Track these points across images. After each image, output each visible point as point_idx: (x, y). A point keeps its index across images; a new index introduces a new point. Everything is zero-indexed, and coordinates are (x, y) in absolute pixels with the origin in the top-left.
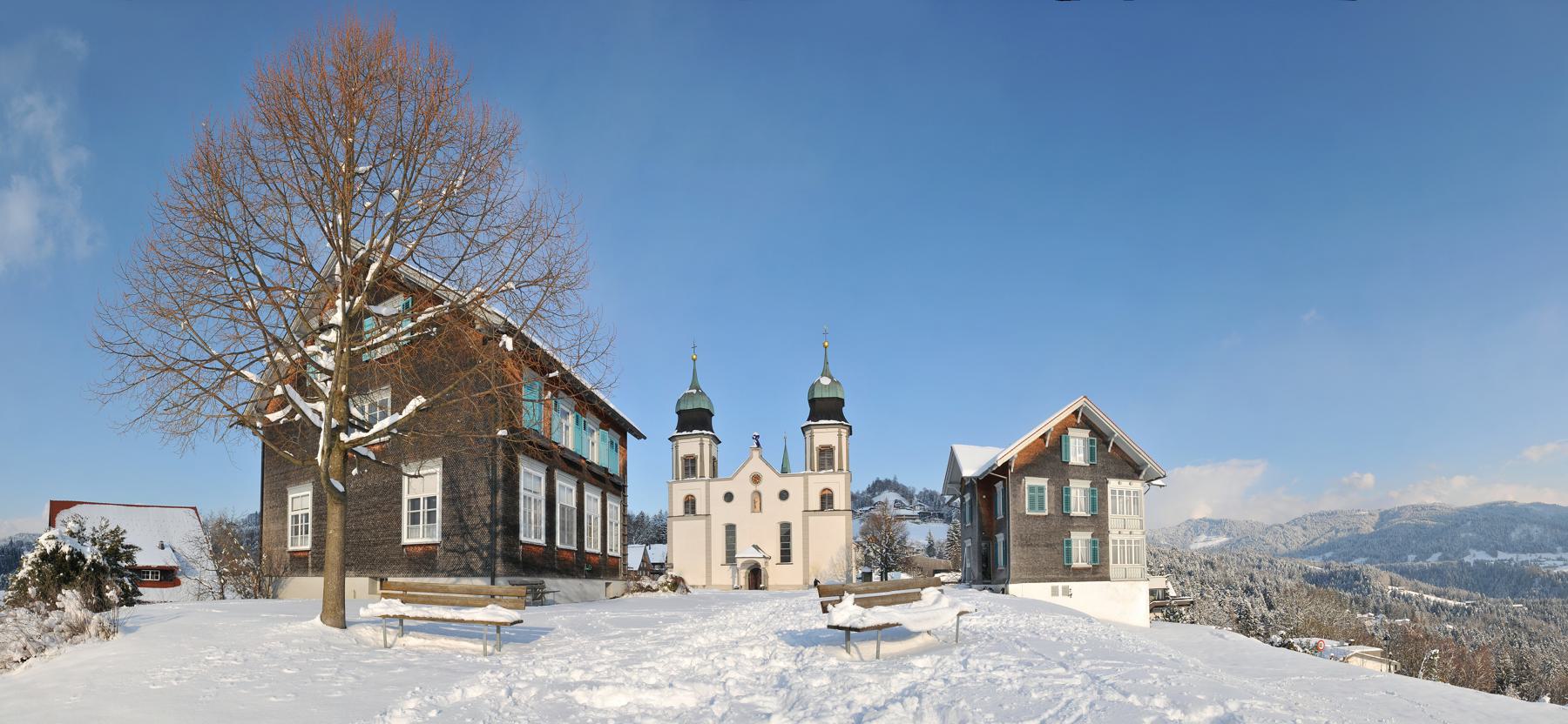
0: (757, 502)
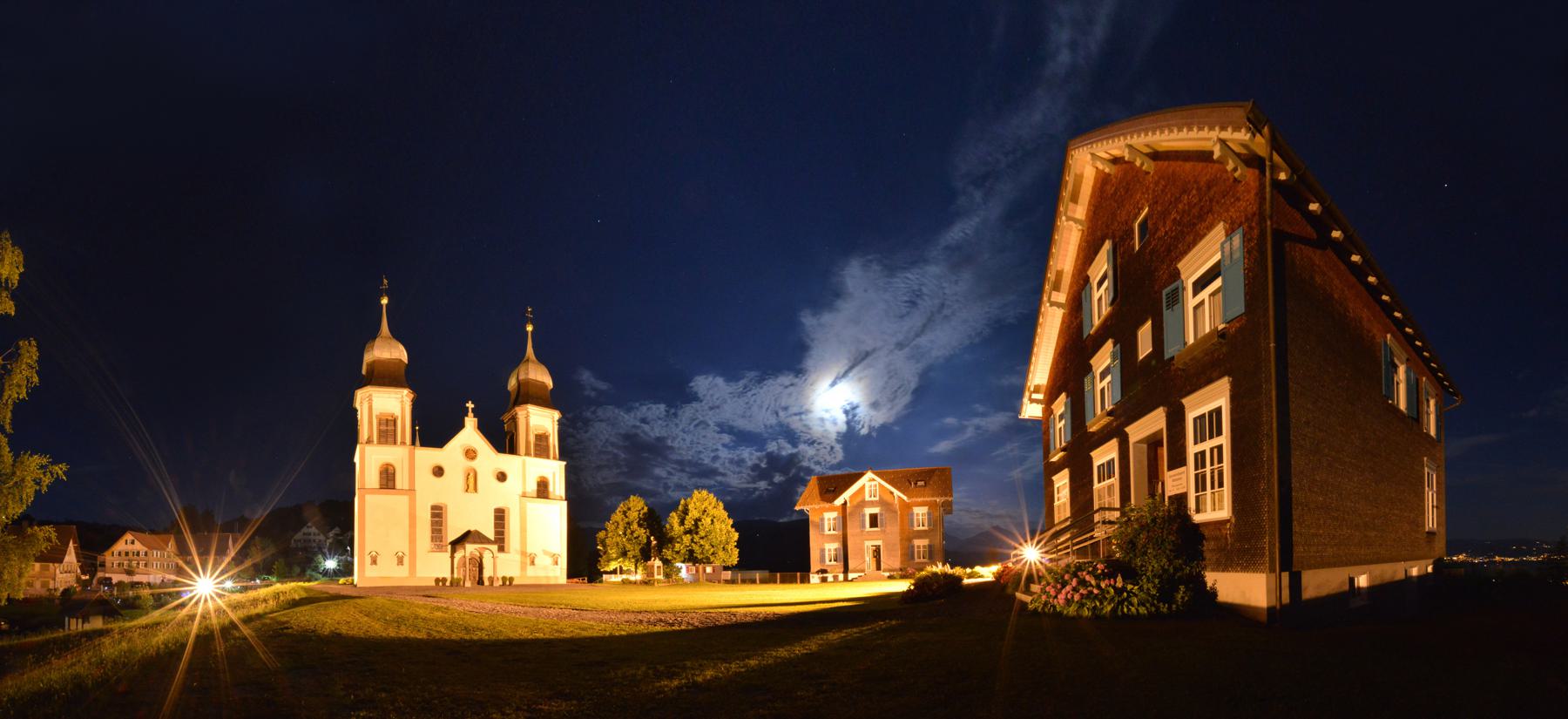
0: (471, 482)
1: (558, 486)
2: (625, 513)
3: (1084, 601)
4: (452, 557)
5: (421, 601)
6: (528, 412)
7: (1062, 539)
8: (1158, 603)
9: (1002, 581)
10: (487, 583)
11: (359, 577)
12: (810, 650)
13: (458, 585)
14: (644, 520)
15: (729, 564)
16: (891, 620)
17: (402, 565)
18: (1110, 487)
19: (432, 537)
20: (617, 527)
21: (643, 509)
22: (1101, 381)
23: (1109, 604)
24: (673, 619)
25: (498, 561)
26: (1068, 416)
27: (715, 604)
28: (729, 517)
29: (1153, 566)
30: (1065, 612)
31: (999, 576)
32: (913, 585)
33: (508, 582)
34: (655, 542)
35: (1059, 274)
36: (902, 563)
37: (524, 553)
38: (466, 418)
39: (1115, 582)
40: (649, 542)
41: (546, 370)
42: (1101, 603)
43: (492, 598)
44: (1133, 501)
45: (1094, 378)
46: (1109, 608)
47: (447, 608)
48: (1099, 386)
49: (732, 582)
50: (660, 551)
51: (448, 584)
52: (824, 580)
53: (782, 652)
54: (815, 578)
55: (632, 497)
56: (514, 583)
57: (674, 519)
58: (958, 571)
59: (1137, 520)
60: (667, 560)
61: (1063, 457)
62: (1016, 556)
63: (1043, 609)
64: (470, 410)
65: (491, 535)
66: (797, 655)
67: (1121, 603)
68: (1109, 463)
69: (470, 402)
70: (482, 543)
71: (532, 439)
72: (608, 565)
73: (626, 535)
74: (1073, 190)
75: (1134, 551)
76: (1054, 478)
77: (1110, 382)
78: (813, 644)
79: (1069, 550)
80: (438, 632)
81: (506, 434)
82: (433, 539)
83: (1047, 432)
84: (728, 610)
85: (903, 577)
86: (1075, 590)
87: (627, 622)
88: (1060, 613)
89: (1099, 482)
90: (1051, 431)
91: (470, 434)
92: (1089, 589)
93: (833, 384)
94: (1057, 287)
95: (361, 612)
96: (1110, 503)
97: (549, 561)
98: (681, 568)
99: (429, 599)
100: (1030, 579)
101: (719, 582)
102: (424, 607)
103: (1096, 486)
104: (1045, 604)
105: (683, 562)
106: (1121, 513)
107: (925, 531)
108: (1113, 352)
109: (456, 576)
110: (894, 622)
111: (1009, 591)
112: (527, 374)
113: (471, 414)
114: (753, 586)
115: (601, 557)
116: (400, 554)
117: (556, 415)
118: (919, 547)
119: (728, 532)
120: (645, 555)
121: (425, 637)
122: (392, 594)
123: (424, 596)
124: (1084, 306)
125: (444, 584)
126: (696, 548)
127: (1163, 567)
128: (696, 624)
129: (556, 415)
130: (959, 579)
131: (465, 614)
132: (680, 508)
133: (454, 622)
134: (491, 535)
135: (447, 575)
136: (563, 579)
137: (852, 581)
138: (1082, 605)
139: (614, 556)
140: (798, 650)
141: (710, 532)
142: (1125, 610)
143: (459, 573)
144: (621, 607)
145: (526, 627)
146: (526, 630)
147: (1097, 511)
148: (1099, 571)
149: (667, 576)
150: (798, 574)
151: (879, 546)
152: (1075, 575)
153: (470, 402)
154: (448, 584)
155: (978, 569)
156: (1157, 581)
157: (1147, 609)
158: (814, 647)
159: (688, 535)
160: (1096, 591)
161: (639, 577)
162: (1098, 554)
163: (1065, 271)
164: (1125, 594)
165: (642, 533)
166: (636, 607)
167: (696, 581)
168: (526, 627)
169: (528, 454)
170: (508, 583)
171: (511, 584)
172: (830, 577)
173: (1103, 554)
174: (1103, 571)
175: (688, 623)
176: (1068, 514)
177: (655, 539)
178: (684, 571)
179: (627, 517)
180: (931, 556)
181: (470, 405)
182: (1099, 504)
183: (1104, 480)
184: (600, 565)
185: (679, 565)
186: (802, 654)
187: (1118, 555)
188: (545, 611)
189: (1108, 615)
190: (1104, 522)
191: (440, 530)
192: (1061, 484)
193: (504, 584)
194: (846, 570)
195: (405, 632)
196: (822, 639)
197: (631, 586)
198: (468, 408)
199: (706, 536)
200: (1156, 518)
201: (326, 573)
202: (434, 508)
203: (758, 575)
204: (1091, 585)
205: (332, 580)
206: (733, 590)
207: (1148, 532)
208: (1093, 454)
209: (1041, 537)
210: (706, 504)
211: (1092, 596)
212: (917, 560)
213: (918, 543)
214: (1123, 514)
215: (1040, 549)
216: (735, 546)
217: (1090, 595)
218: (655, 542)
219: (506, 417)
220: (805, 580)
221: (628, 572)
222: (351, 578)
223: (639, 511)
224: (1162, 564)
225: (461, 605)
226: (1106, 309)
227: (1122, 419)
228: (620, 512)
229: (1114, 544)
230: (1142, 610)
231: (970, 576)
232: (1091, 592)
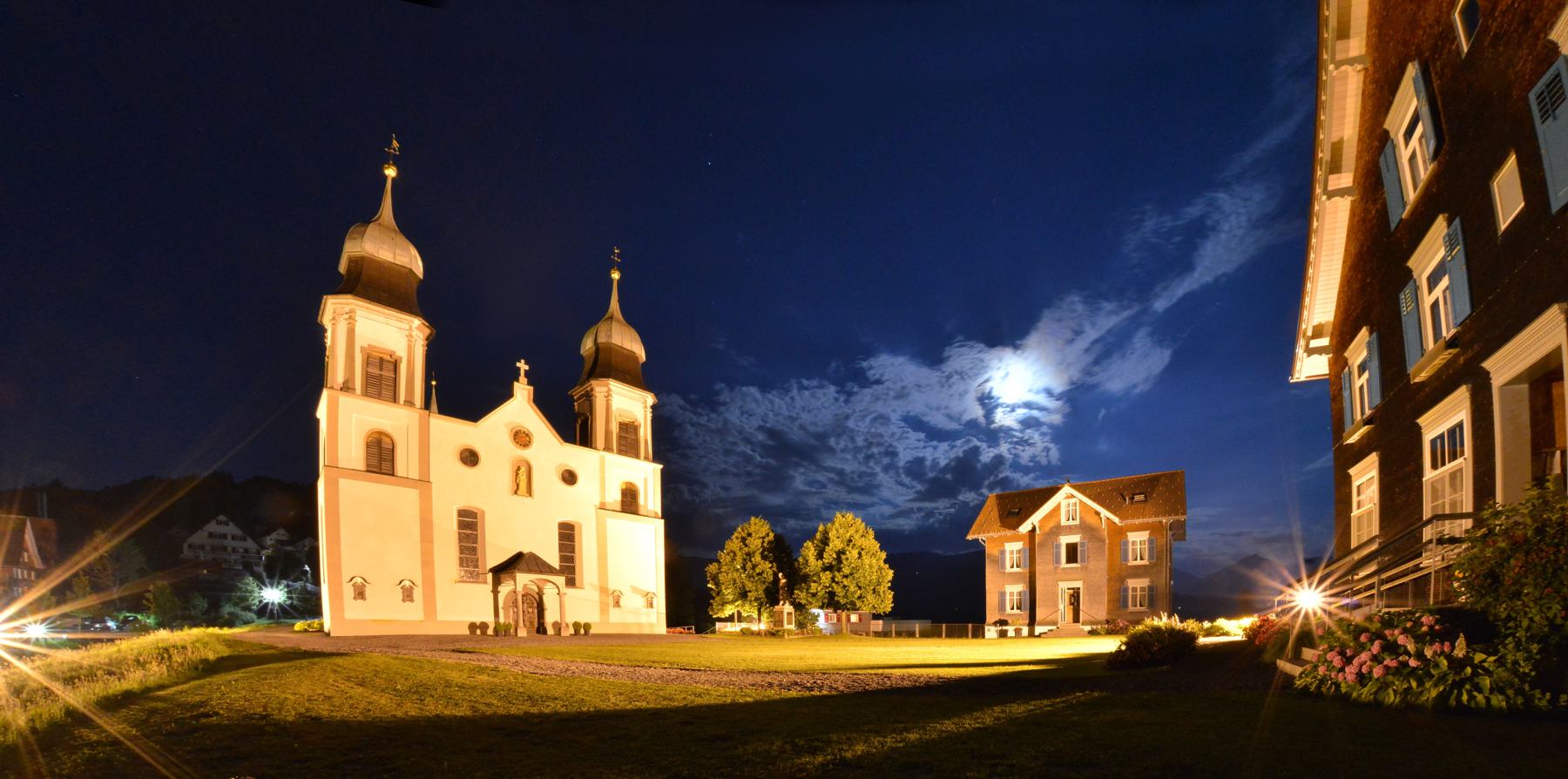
0: (523, 479)
1: (651, 498)
2: (743, 540)
3: (1390, 678)
4: (495, 592)
5: (453, 659)
6: (609, 390)
7: (1362, 574)
8: (1532, 688)
9: (1257, 643)
10: (550, 631)
11: (333, 618)
12: (984, 723)
13: (507, 633)
14: (770, 550)
15: (881, 611)
16: (1092, 691)
17: (412, 600)
18: (1455, 476)
19: (461, 560)
20: (733, 559)
21: (768, 535)
22: (1430, 291)
23: (1436, 685)
24: (812, 681)
25: (566, 600)
26: (1375, 364)
27: (863, 663)
28: (881, 548)
29: (1531, 620)
30: (1355, 695)
31: (1253, 634)
32: (1125, 644)
33: (582, 630)
34: (784, 581)
35: (1337, 148)
36: (1109, 613)
37: (603, 590)
38: (516, 384)
39: (1453, 648)
40: (776, 580)
41: (639, 338)
42: (1421, 683)
43: (562, 653)
44: (1499, 498)
45: (1417, 289)
46: (1434, 693)
47: (496, 669)
48: (1427, 301)
49: (885, 634)
50: (790, 592)
51: (490, 632)
52: (1003, 634)
53: (949, 725)
54: (991, 632)
55: (753, 518)
56: (592, 631)
57: (809, 550)
58: (1191, 625)
59: (1506, 532)
60: (800, 604)
61: (1368, 434)
62: (1281, 603)
63: (1319, 687)
64: (522, 373)
65: (554, 560)
66: (967, 730)
67: (1458, 685)
68: (1452, 432)
69: (523, 361)
70: (541, 572)
71: (615, 428)
72: (722, 610)
73: (745, 570)
74: (1339, 23)
75: (1496, 590)
76: (1352, 471)
77: (1447, 288)
78: (988, 717)
79: (1374, 591)
80: (487, 705)
81: (576, 416)
82: (462, 562)
83: (1337, 397)
84: (880, 671)
85: (1112, 632)
86: (1376, 659)
87: (753, 685)
88: (1347, 696)
89: (1434, 466)
90: (1346, 394)
91: (520, 407)
92: (1401, 658)
93: (998, 398)
94: (1335, 167)
95: (348, 679)
96: (1453, 504)
97: (640, 602)
98: (818, 615)
99: (463, 656)
100: (1306, 638)
101: (867, 634)
102: (459, 667)
103: (1429, 474)
104: (1322, 681)
105: (822, 608)
106: (1475, 521)
107: (1145, 566)
108: (1448, 235)
109: (502, 620)
110: (1096, 694)
111: (1267, 657)
112: (610, 336)
113: (523, 379)
114: (911, 641)
115: (714, 598)
116: (407, 583)
117: (650, 399)
118: (1134, 589)
119: (880, 569)
120: (772, 597)
121: (468, 713)
122: (398, 648)
123: (453, 651)
124: (1385, 181)
125: (484, 633)
126: (838, 589)
127: (1551, 622)
128: (841, 688)
129: (650, 399)
130: (1192, 637)
131: (526, 677)
132: (818, 536)
133: (510, 689)
134: (554, 560)
135: (489, 619)
136: (661, 627)
137: (1039, 636)
138: (1384, 686)
139: (730, 597)
140: (969, 723)
141: (856, 569)
142: (1465, 697)
143: (506, 616)
144: (742, 666)
145: (621, 694)
146: (622, 698)
147: (1429, 521)
148: (1425, 629)
149: (801, 625)
150: (970, 625)
151: (1079, 589)
152: (1379, 635)
153: (523, 361)
154: (490, 632)
155: (1221, 622)
156: (1535, 647)
157: (1508, 699)
158: (988, 721)
159: (828, 573)
160: (1413, 663)
161: (763, 626)
162: (1425, 595)
163: (1345, 138)
164: (1469, 670)
165: (766, 567)
166: (762, 666)
167: (837, 633)
168: (621, 694)
169: (608, 448)
170: (582, 631)
171: (586, 633)
172: (1011, 631)
173: (1436, 596)
174: (1431, 627)
175: (831, 687)
176: (1375, 531)
177: (785, 576)
178: (822, 619)
179: (746, 546)
180: (1153, 602)
181: (523, 366)
182: (1434, 508)
183: (1443, 464)
184: (713, 610)
185: (815, 611)
186: (975, 729)
187: (1463, 599)
188: (643, 671)
189: (1430, 705)
190: (1440, 541)
191: (474, 550)
192: (1364, 479)
193: (577, 632)
194: (1032, 622)
195: (433, 708)
196: (1003, 712)
197: (752, 639)
198: (519, 369)
199: (851, 574)
200: (1544, 526)
201: (264, 610)
202: (462, 513)
203: (917, 626)
204: (1407, 652)
205: (278, 623)
206: (886, 646)
207: (1527, 553)
208: (1421, 421)
209: (1328, 570)
210: (852, 531)
211: (1406, 671)
212: (1131, 608)
213: (1132, 583)
214: (1478, 523)
215: (1324, 590)
216: (890, 588)
217: (1402, 670)
218: (784, 581)
219: (577, 392)
220: (979, 633)
221: (749, 619)
222: (316, 621)
223: (763, 538)
224: (1550, 615)
225: (516, 663)
226: (1426, 169)
227: (1476, 348)
228: (737, 538)
229: (1458, 580)
230: (1498, 701)
231: (1209, 633)
232: (1405, 664)
